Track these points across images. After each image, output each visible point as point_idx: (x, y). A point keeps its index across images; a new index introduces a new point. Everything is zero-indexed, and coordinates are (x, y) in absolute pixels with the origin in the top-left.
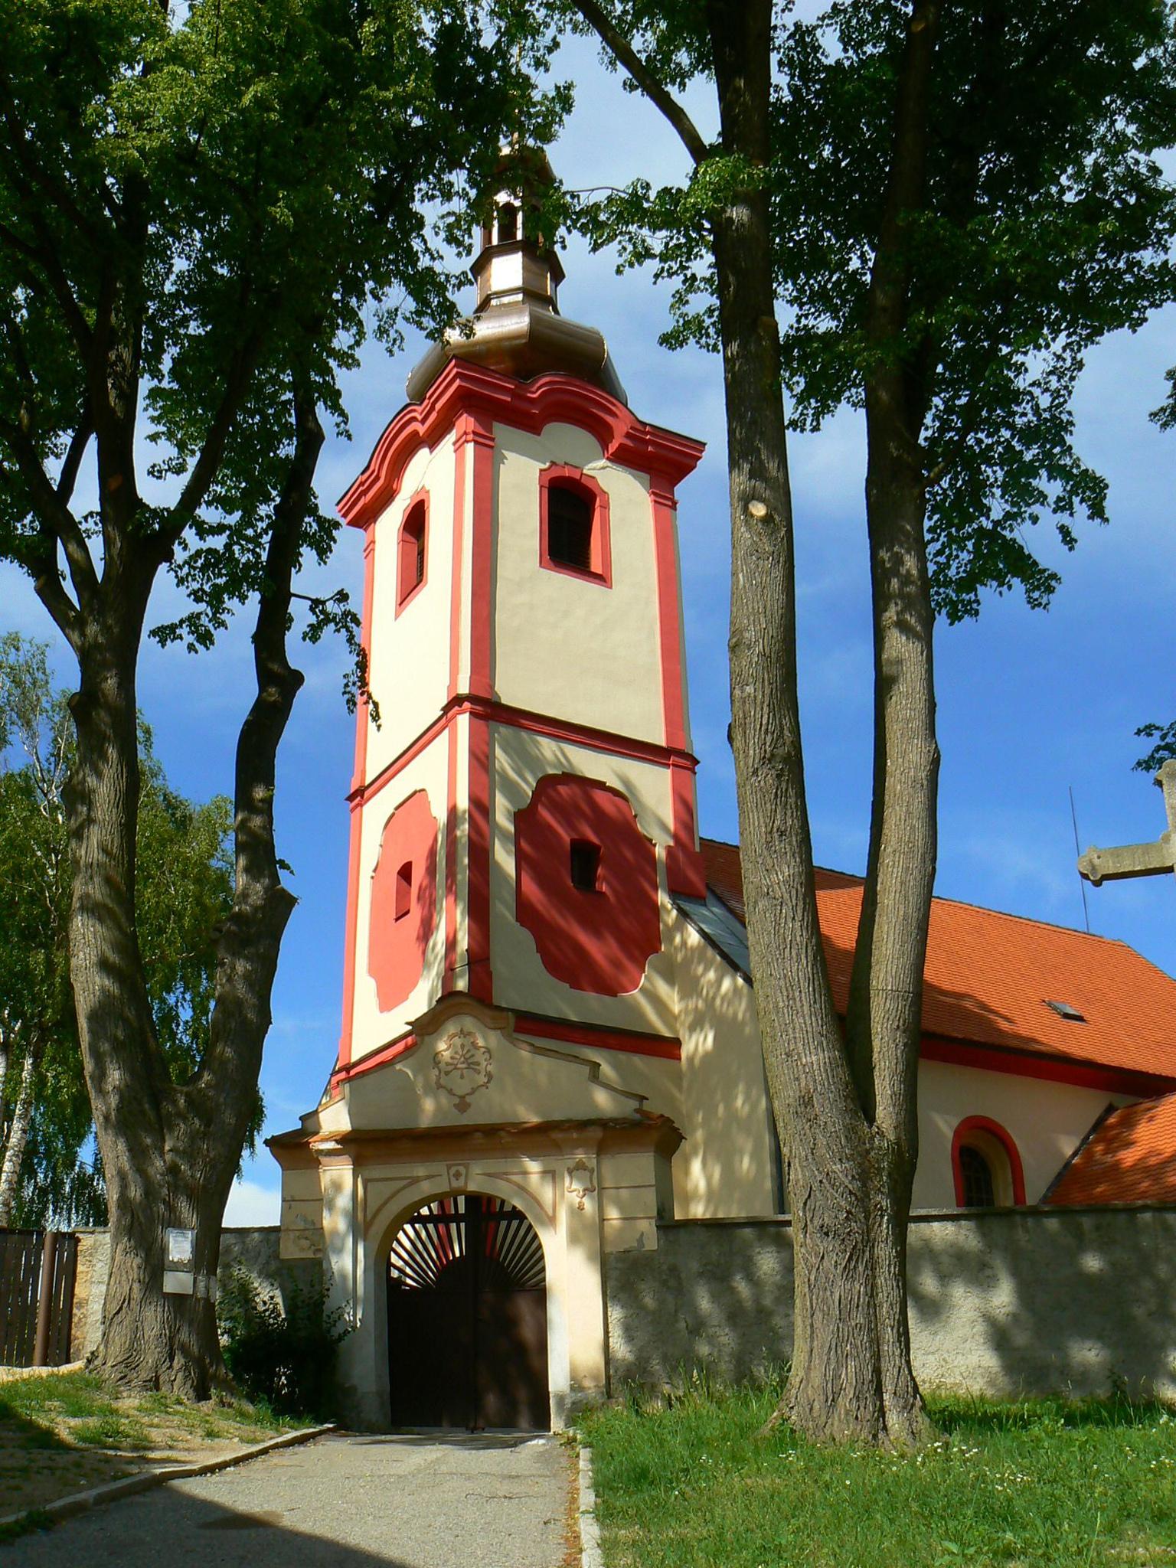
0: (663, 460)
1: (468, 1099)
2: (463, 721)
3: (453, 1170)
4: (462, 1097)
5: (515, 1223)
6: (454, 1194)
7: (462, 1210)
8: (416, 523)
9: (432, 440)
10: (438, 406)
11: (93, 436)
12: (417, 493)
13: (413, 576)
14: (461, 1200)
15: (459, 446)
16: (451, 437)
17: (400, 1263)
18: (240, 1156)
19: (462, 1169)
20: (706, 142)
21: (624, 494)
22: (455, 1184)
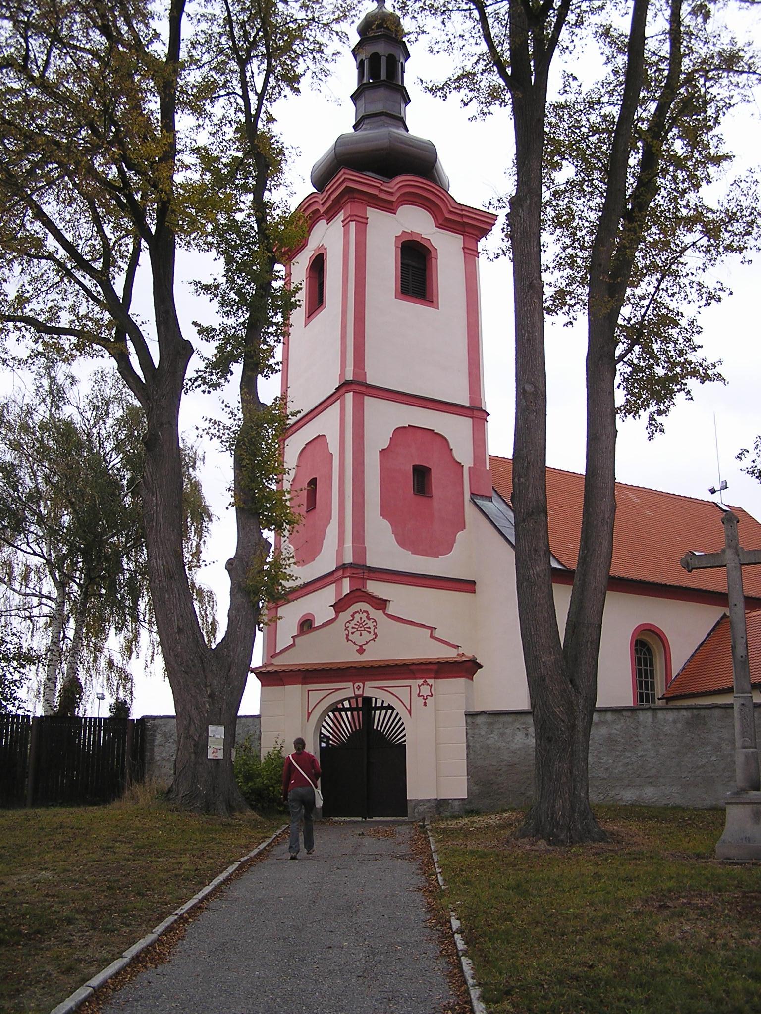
0: (470, 225)
1: (364, 647)
2: (349, 396)
3: (356, 685)
4: (361, 646)
5: (390, 711)
6: (356, 697)
7: (360, 705)
8: (318, 265)
9: (330, 215)
10: (333, 197)
11: (143, 240)
12: (319, 248)
13: (317, 301)
14: (360, 700)
15: (346, 225)
16: (341, 216)
17: (328, 734)
18: (324, 800)
19: (361, 685)
20: (552, 461)
21: (447, 247)
22: (357, 692)
